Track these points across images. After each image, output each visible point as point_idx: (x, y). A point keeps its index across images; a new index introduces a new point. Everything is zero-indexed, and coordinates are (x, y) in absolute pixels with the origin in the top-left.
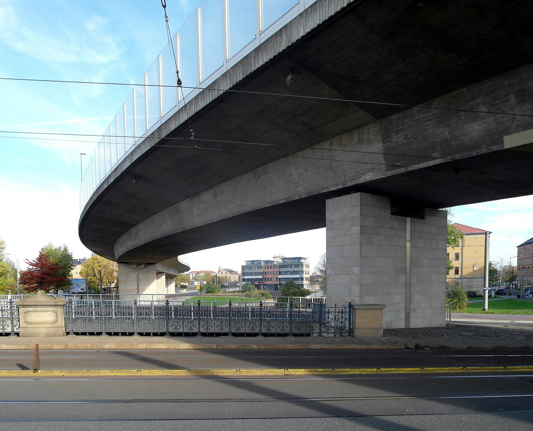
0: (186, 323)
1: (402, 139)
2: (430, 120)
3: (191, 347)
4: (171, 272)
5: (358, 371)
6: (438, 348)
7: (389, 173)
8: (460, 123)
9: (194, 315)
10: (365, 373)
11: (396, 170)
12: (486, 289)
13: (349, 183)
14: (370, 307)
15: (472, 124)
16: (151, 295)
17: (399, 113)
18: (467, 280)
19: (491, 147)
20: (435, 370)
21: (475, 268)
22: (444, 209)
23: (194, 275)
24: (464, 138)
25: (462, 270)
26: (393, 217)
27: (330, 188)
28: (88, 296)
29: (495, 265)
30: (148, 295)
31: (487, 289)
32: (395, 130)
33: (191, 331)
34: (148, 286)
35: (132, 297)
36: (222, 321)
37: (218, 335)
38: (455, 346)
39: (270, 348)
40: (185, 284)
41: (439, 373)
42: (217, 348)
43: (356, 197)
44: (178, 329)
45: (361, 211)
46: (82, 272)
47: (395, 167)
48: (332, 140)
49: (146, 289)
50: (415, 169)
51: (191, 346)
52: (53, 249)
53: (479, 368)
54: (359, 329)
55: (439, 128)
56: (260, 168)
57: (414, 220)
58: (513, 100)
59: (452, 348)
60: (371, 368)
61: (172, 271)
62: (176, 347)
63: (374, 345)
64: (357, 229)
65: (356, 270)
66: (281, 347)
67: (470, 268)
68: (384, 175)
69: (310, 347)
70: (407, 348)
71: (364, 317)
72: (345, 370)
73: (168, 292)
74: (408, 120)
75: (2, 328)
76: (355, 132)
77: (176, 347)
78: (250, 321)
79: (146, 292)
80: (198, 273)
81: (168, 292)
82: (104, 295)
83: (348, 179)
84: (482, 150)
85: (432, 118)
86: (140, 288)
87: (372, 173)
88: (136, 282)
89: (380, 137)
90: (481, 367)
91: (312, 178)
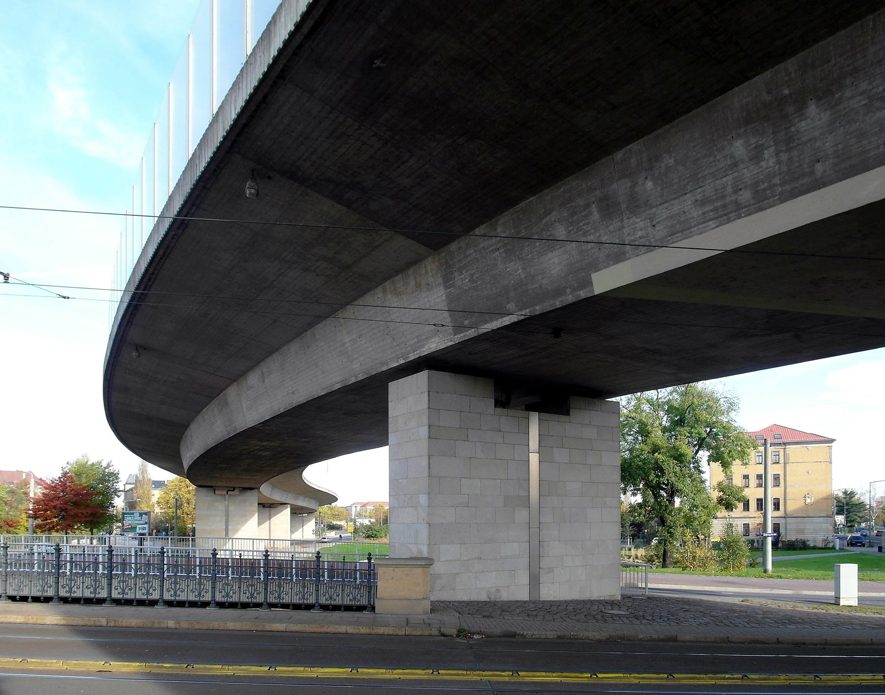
0: (244, 587)
1: (467, 281)
2: (498, 249)
3: (62, 622)
4: (301, 503)
5: (479, 675)
6: (500, 637)
7: (459, 338)
8: (535, 253)
9: (233, 573)
10: (245, 673)
11: (466, 333)
12: (767, 535)
13: (412, 356)
14: (402, 562)
15: (550, 255)
16: (258, 540)
17: (459, 240)
18: (794, 521)
19: (578, 293)
20: (377, 673)
21: (808, 501)
22: (613, 399)
23: (358, 509)
24: (543, 278)
25: (785, 502)
26: (499, 410)
27: (390, 363)
28: (170, 539)
29: (862, 494)
30: (243, 540)
31: (769, 535)
32: (457, 266)
33: (123, 596)
34: (243, 526)
35: (204, 541)
36: (305, 583)
37: (245, 606)
38: (534, 633)
39: (197, 627)
40: (339, 523)
41: (382, 679)
42: (107, 624)
43: (422, 377)
44: (358, 600)
45: (429, 401)
46: (159, 500)
47: (464, 328)
48: (385, 286)
49: (240, 529)
50: (488, 330)
51: (63, 619)
52: (90, 463)
53: (465, 672)
54: (384, 599)
55: (510, 263)
56: (308, 332)
57: (545, 416)
58: (596, 215)
59: (528, 637)
60: (261, 666)
61: (304, 501)
62: (38, 621)
63: (382, 628)
64: (424, 431)
65: (423, 499)
66: (216, 627)
67: (800, 499)
68: (452, 341)
69: (268, 627)
70: (444, 635)
71: (392, 579)
72: (211, 666)
73: (303, 536)
74: (471, 251)
75: (68, 590)
76: (411, 271)
77: (39, 622)
78: (328, 585)
79: (239, 535)
80: (364, 505)
81: (303, 536)
82: (183, 539)
83: (409, 348)
84: (567, 297)
85: (500, 246)
86: (230, 527)
87: (436, 339)
88: (224, 519)
89: (440, 280)
90: (467, 670)
91: (367, 348)
